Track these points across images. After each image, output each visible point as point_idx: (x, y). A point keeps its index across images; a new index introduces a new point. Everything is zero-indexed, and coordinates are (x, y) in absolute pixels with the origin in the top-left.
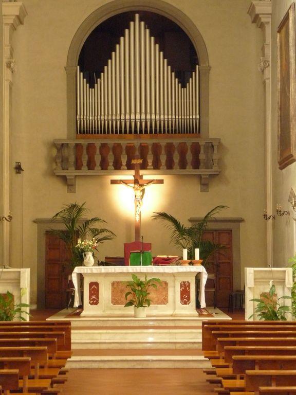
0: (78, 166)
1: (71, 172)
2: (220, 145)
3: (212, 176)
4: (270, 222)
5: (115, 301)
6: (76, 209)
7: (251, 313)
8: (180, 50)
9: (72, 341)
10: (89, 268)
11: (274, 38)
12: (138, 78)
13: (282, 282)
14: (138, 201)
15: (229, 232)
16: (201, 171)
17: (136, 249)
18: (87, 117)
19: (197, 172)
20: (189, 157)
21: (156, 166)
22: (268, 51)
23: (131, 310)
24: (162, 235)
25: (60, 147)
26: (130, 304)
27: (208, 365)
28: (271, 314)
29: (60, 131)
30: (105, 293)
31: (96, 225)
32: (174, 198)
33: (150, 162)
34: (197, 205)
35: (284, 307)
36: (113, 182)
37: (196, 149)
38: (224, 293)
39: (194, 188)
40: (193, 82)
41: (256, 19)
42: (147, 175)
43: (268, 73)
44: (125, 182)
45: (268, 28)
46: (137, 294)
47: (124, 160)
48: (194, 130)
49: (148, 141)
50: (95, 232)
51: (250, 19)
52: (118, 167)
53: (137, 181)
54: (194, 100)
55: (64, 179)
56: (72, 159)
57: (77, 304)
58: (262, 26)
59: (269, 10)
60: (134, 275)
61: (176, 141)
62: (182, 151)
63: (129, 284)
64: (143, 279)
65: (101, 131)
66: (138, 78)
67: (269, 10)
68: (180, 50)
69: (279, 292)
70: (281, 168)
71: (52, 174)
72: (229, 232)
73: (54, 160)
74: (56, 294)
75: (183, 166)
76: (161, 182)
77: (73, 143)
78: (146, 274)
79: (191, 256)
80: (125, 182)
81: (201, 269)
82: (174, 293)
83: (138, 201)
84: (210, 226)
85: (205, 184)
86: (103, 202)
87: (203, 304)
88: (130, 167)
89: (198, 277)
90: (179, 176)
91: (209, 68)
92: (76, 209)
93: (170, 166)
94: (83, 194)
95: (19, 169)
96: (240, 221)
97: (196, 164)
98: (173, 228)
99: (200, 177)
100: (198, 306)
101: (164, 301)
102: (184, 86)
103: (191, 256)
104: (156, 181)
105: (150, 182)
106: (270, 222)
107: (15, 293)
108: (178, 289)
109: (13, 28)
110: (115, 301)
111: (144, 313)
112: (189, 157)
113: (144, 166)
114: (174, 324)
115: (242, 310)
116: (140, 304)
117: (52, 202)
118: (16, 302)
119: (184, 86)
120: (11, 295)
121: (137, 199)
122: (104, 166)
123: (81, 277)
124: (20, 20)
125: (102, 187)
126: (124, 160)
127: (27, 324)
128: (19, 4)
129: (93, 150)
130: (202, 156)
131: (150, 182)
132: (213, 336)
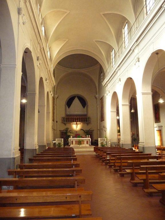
0: (67, 121)
1: (65, 122)
2: (90, 118)
3: (89, 123)
4: (99, 131)
5: (76, 144)
6: (67, 129)
7: (99, 145)
8: (83, 102)
9: (140, 141)
10: (71, 139)
11: (99, 101)
12: (76, 108)
13: (104, 140)
14: (77, 127)
15: (92, 132)
16: (88, 122)
17: (77, 135)
18: (68, 113)
19: (86, 122)
20: (85, 120)
21: (80, 121)
22: (98, 103)
23: (79, 145)
24: (82, 133)
25: (63, 118)
26: (78, 144)
27: (96, 154)
28: (103, 145)
29: (64, 116)
30: (74, 142)
31: (71, 131)
32: (83, 127)
33: (79, 121)
34: (87, 128)
35: (105, 144)
36: (73, 124)
37: (86, 118)
38: (94, 143)
39: (86, 125)
40: (86, 107)
41: (96, 98)
42: (78, 123)
43: (98, 106)
44: (74, 124)
45: (98, 99)
46: (80, 143)
47: (74, 120)
48: (86, 115)
49: (78, 117)
50: (71, 132)
51: (95, 98)
52: (73, 121)
53: (77, 124)
54: (86, 110)
55: (64, 123)
56: (66, 120)
57: (69, 144)
58: (97, 99)
59: (98, 96)
60: (79, 140)
61: (83, 117)
62: (83, 119)
63: (78, 141)
64: (80, 140)
65: (71, 115)
66: (76, 108)
67: (98, 96)
68: (83, 102)
69: (104, 142)
70: (101, 122)
71: (62, 123)
72: (92, 132)
73: (62, 120)
74: (66, 143)
75: (84, 121)
76: (81, 124)
77: (66, 117)
78: (81, 139)
79: (88, 136)
80: (74, 124)
81: (90, 138)
82: (85, 142)
83: (77, 127)
84: (89, 131)
85: (88, 124)
86: (71, 127)
87: (90, 144)
88: (75, 121)
89: (89, 140)
90: (83, 123)
91: (88, 106)
92: (67, 129)
93: (82, 121)
94: (68, 126)
95: (57, 122)
96: (93, 130)
97: (86, 121)
98: (83, 131)
99: (87, 123)
100: (89, 145)
101: (84, 144)
102: (84, 108)
103: (88, 136)
104: (135, 136)
105: (79, 124)
106: (99, 131)
107: (61, 143)
108: (86, 142)
109: (56, 99)
110: (76, 144)
111: (81, 146)
112: (85, 120)
113: (78, 121)
114: (86, 147)
115: (98, 145)
116: (80, 144)
117: (63, 128)
118: (61, 144)
119: (84, 108)
120: (60, 143)
121: (77, 127)
122: (71, 121)
123: (70, 140)
124: (57, 98)
125: (71, 125)
126: (74, 120)
127: (47, 150)
128: (58, 95)
129: (69, 119)
130: (87, 120)
131: (79, 124)
132: (96, 150)
